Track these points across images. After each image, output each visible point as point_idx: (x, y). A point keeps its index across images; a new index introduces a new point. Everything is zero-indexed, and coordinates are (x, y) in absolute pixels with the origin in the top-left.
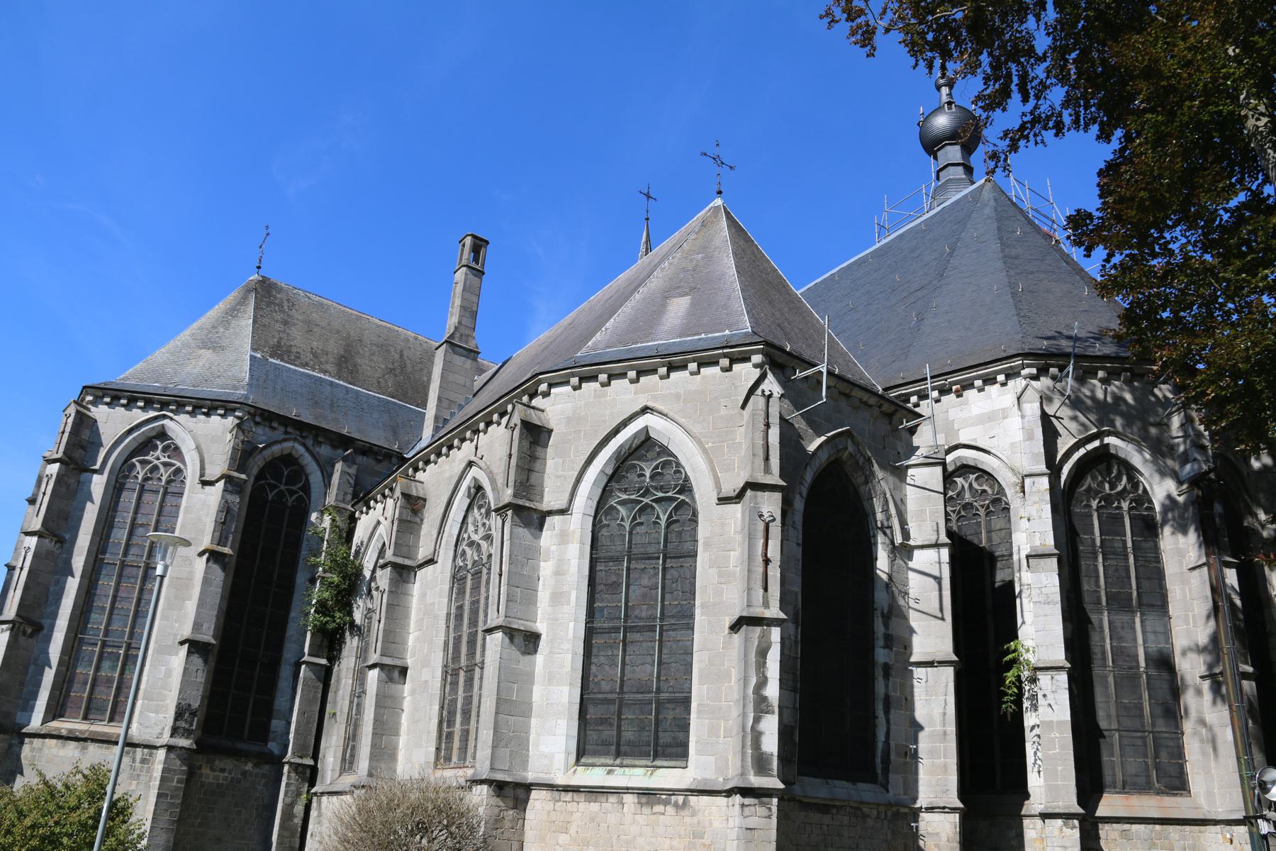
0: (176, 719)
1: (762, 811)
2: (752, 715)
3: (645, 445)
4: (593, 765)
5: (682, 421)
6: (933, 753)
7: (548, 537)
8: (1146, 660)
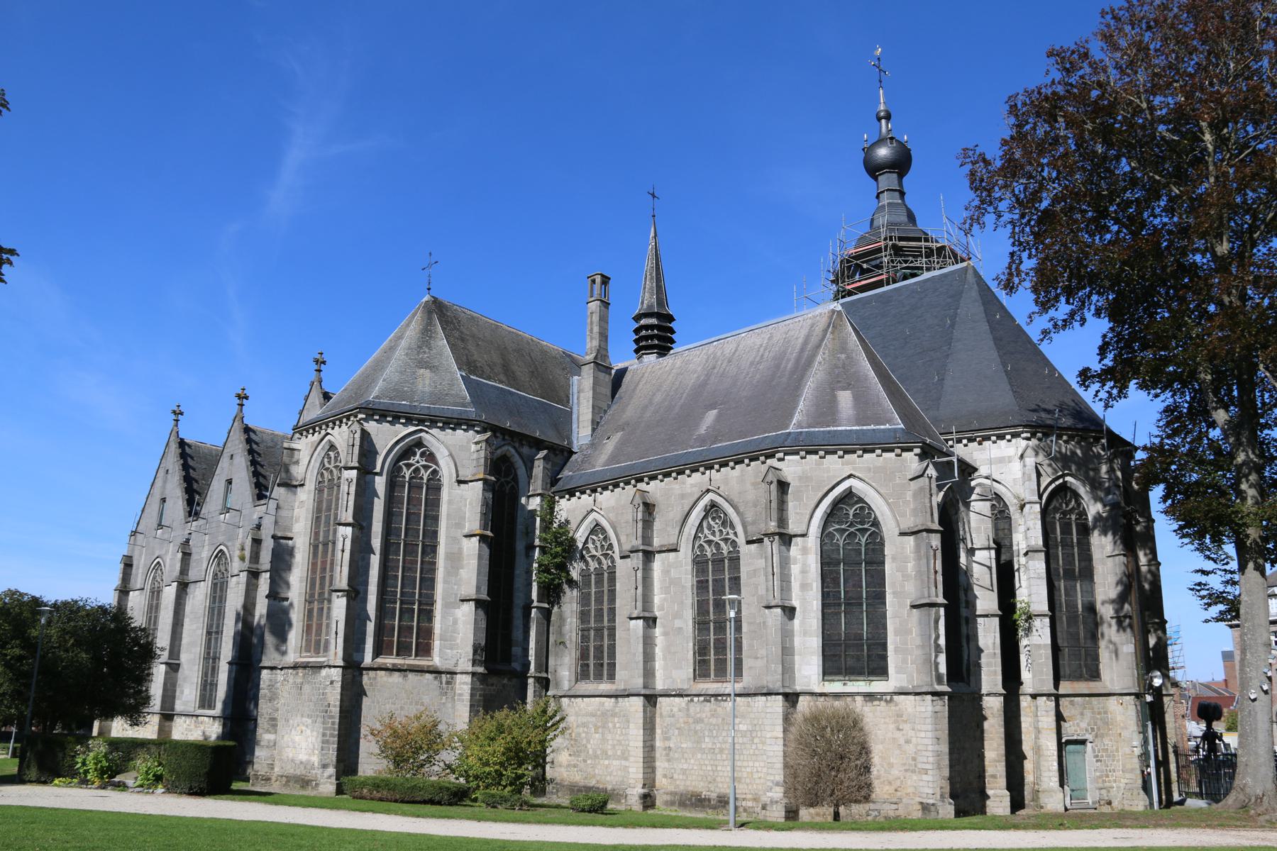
0: (474, 655)
1: (940, 703)
2: (934, 654)
3: (849, 497)
4: (833, 681)
5: (873, 484)
6: (989, 665)
7: (794, 550)
8: (1082, 607)
